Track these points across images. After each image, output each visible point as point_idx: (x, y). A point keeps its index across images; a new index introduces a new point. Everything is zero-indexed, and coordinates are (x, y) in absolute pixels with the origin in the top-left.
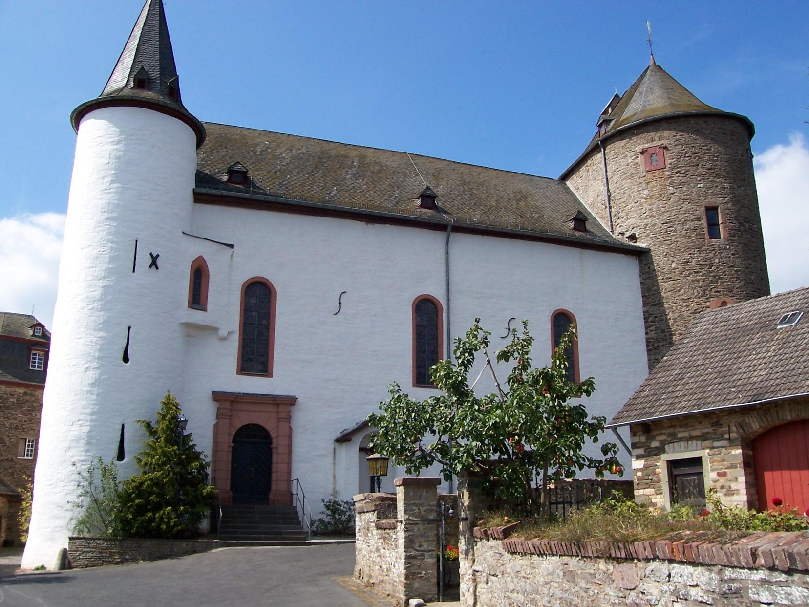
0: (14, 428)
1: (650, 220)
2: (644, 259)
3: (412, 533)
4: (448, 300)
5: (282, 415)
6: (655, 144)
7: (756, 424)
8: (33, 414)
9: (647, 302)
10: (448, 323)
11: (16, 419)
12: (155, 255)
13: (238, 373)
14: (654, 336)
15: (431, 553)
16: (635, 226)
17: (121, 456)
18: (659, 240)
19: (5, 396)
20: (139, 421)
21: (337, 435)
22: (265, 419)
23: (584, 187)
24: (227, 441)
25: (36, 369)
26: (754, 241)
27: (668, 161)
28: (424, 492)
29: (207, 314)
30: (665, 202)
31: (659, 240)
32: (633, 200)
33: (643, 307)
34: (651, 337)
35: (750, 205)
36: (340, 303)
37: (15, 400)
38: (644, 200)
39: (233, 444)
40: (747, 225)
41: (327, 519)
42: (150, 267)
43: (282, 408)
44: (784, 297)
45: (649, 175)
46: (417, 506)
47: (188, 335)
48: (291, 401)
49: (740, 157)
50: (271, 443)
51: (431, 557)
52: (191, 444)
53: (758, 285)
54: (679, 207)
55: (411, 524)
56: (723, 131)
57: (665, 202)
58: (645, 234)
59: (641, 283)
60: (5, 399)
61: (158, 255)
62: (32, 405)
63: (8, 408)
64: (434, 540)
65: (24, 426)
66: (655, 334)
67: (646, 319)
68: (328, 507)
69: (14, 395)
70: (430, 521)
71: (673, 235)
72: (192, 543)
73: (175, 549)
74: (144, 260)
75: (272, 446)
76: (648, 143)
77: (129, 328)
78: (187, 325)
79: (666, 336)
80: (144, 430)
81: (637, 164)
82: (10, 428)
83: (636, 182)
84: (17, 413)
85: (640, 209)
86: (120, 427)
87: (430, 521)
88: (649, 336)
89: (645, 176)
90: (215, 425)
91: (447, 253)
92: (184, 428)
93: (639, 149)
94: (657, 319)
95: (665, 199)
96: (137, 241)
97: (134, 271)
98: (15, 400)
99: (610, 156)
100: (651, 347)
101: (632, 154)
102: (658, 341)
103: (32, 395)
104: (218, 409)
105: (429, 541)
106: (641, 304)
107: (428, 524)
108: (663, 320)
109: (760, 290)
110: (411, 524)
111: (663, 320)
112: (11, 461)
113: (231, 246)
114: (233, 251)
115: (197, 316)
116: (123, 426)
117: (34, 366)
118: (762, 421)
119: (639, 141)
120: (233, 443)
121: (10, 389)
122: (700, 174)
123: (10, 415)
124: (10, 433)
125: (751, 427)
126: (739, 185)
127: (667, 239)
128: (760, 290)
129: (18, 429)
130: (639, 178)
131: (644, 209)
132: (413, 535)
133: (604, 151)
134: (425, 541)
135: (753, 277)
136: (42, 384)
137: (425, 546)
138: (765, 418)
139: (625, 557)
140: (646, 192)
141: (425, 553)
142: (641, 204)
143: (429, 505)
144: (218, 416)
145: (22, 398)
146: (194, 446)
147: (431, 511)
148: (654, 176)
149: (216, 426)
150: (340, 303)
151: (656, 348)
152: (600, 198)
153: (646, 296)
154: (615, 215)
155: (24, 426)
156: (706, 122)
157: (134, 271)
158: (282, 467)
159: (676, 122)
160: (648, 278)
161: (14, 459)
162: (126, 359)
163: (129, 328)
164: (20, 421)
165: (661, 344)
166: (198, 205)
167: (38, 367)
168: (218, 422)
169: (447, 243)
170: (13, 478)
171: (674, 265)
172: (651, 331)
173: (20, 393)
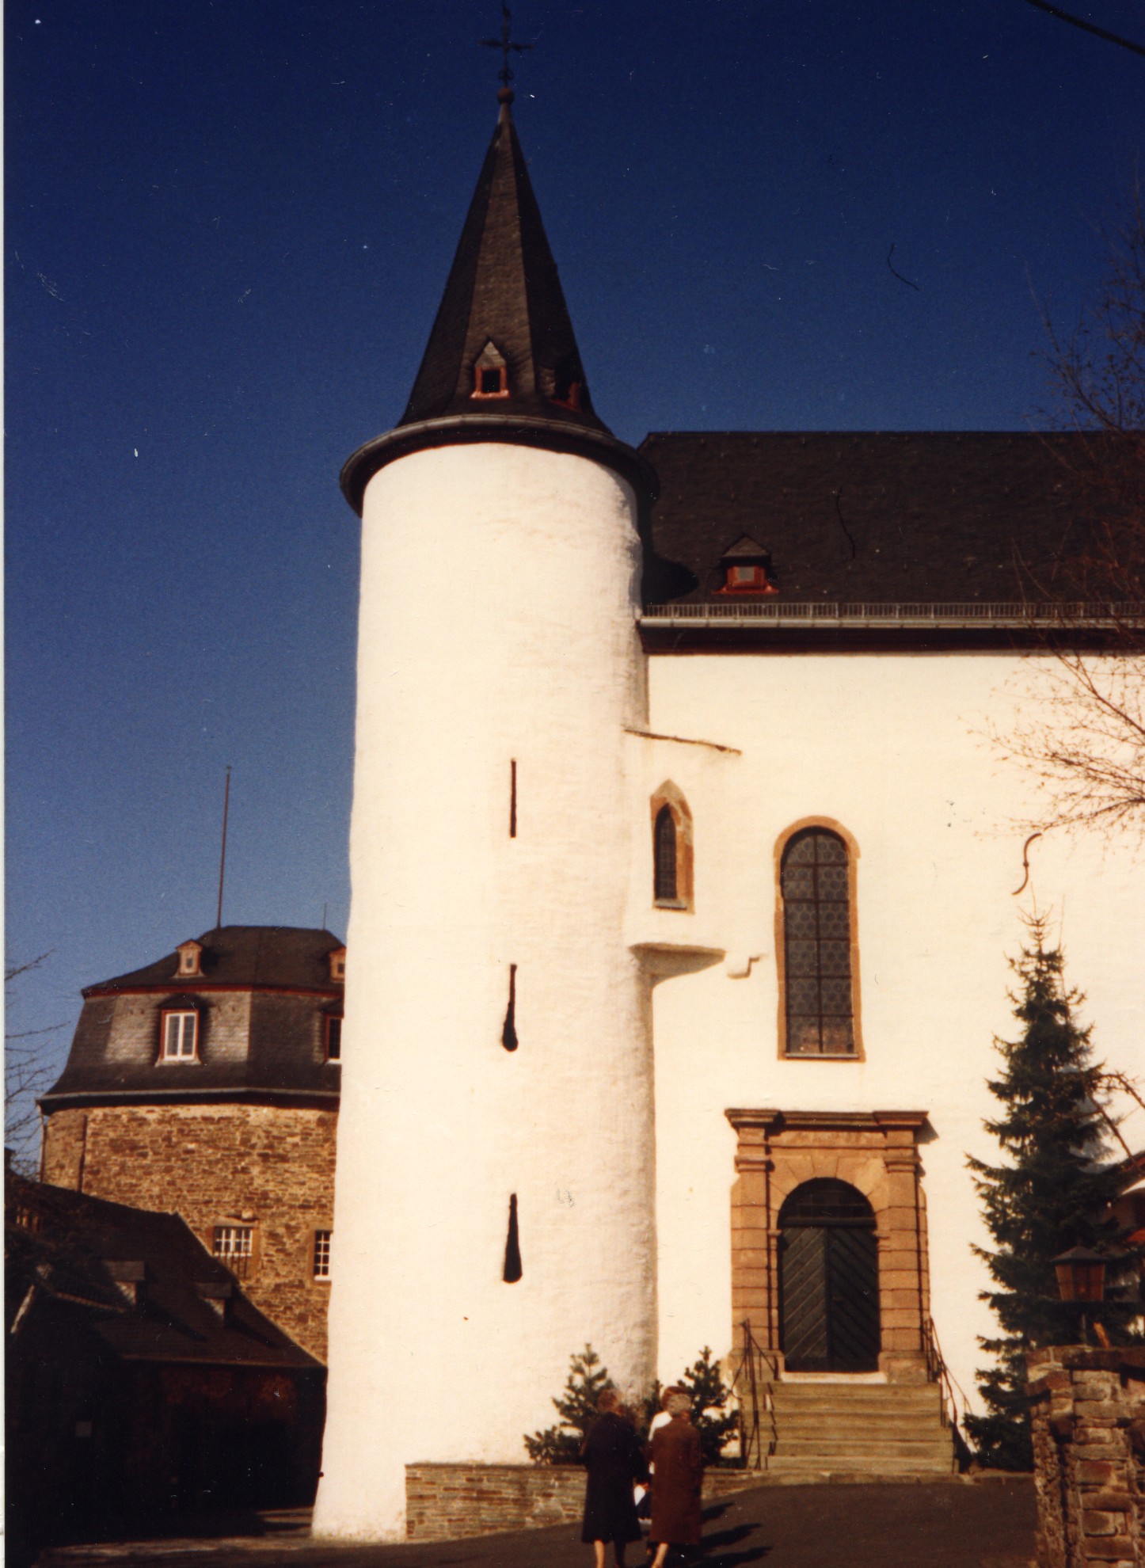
13: (860, 1058)
37: (297, 1139)
50: (874, 1226)
63: (284, 1159)
75: (877, 1233)
77: (513, 968)
86: (508, 1203)
97: (513, 833)
112: (297, 1287)
116: (514, 1200)
124: (292, 1219)
136: (329, 1094)
139: (762, 1133)
157: (513, 833)
162: (510, 1040)
163: (513, 968)
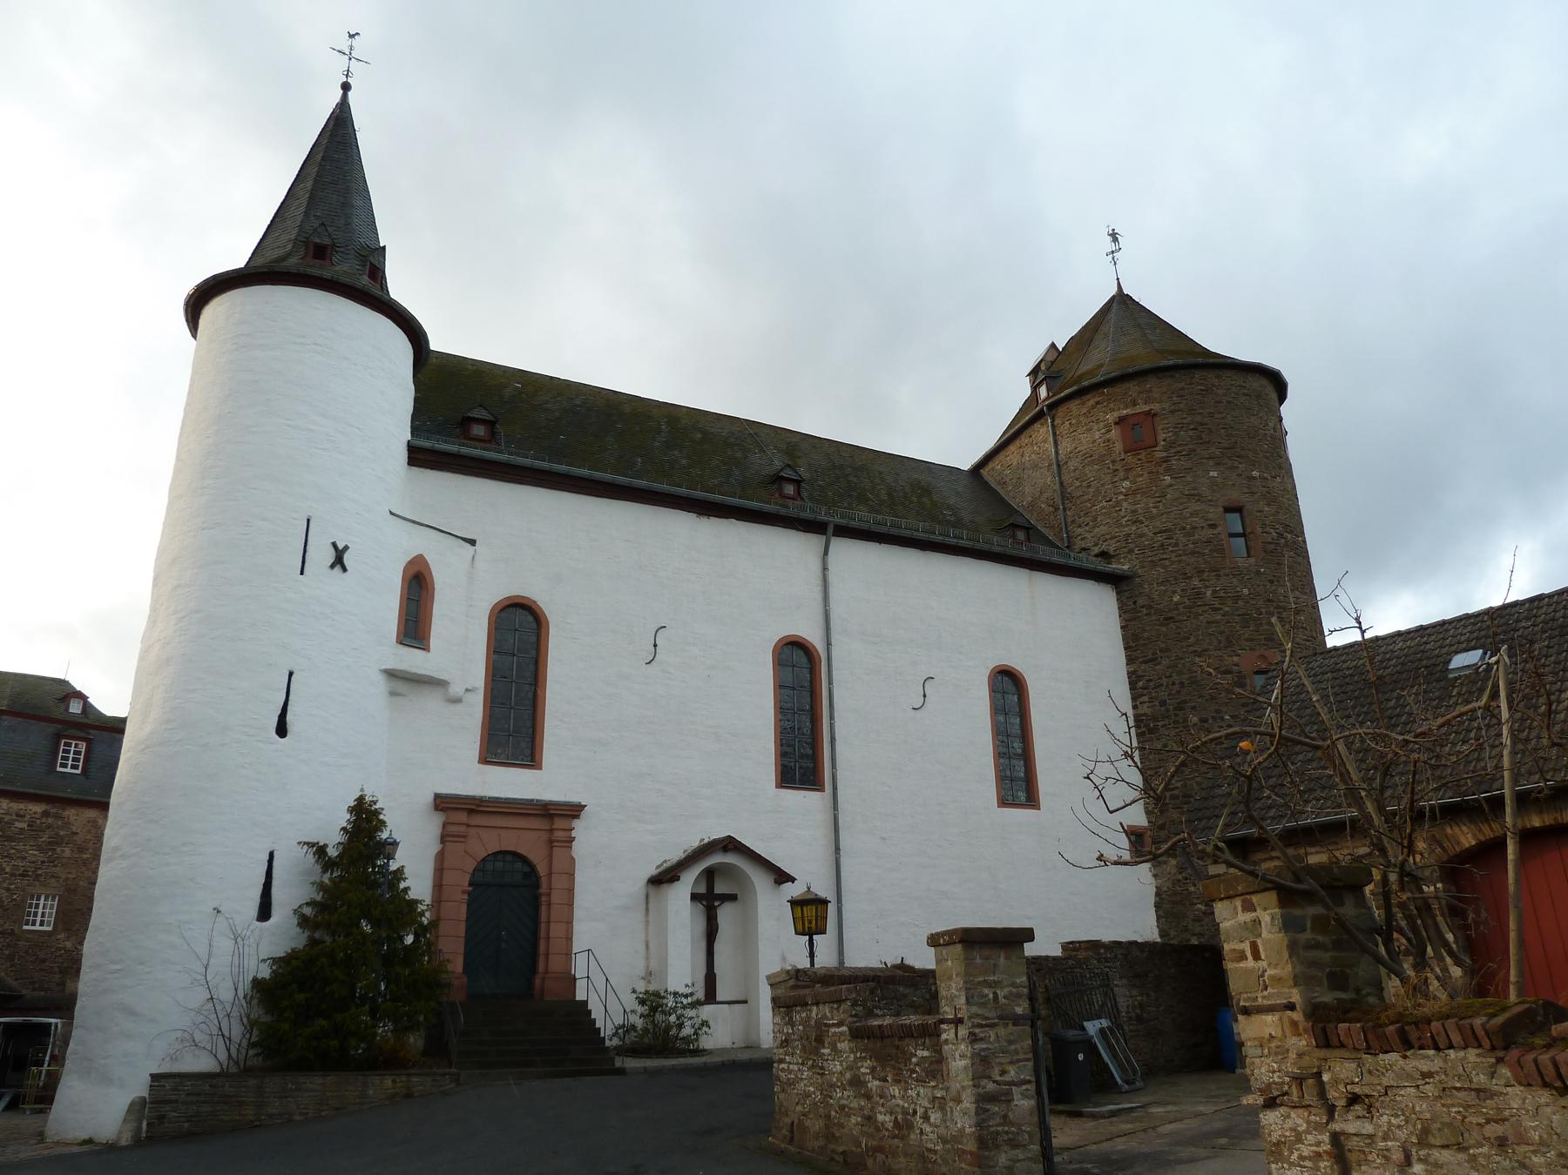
0: (20, 875)
1: (1134, 528)
2: (1125, 588)
3: (984, 1046)
4: (829, 644)
5: (559, 835)
6: (1138, 409)
7: (1469, 836)
8: (58, 850)
9: (1133, 657)
10: (830, 682)
11: (25, 858)
12: (341, 547)
14: (1148, 711)
15: (1024, 1087)
16: (1108, 537)
17: (265, 912)
18: (1150, 559)
19: (7, 818)
20: (305, 843)
21: (652, 871)
22: (528, 842)
23: (1014, 481)
24: (460, 881)
25: (68, 770)
26: (1299, 561)
27: (1161, 436)
28: (1002, 960)
29: (429, 655)
30: (1159, 499)
31: (1150, 559)
32: (1104, 497)
33: (1127, 665)
34: (1143, 712)
35: (1290, 505)
36: (655, 646)
37: (25, 825)
38: (1122, 497)
39: (471, 889)
40: (1289, 536)
41: (639, 1023)
42: (332, 566)
43: (559, 823)
44: (1434, 630)
45: (1130, 459)
46: (990, 987)
47: (393, 694)
48: (574, 811)
49: (1272, 432)
51: (1025, 1096)
52: (402, 885)
53: (1311, 631)
54: (1181, 507)
55: (981, 1026)
56: (1246, 391)
57: (1159, 499)
58: (1126, 550)
59: (1122, 627)
60: (7, 823)
61: (346, 548)
62: (57, 834)
64: (1028, 1060)
65: (40, 872)
66: (1148, 707)
67: (1133, 685)
68: (642, 1002)
69: (24, 816)
70: (1016, 1020)
71: (1172, 551)
72: (404, 1078)
73: (371, 1092)
74: (321, 555)
76: (1127, 408)
77: (291, 674)
78: (391, 674)
79: (1168, 710)
80: (311, 858)
81: (1108, 441)
82: (12, 875)
83: (1109, 468)
84: (28, 847)
85: (1116, 511)
87: (1016, 1020)
88: (1140, 711)
89: (1124, 460)
90: (437, 854)
91: (825, 569)
92: (390, 857)
93: (1111, 417)
94: (1151, 684)
95: (1157, 495)
96: (308, 520)
97: (302, 573)
98: (25, 825)
99: (1063, 429)
100: (1144, 729)
101: (1102, 425)
102: (1155, 719)
103: (57, 817)
104: (445, 825)
105: (1019, 1061)
106: (1123, 660)
107: (1014, 1025)
108: (1162, 685)
109: (1315, 639)
110: (981, 1026)
111: (1162, 685)
112: (9, 934)
113: (472, 542)
114: (475, 551)
115: (412, 660)
116: (271, 855)
117: (63, 765)
118: (1480, 830)
119: (1112, 405)
120: (470, 885)
121: (16, 806)
122: (1213, 455)
123: (12, 851)
125: (1458, 843)
126: (1273, 474)
127: (1165, 556)
128: (1315, 639)
129: (28, 876)
130: (1114, 462)
131: (1123, 510)
132: (988, 1049)
133: (1052, 422)
134: (1012, 1063)
135: (1302, 618)
137: (1012, 1073)
138: (1486, 826)
140: (1126, 484)
141: (1013, 1088)
142: (1118, 503)
143: (1013, 985)
144: (443, 839)
145: (38, 821)
146: (406, 889)
147: (1019, 996)
148: (1139, 460)
149: (440, 858)
150: (655, 646)
151: (1151, 731)
152: (1046, 495)
153: (1131, 647)
154: (1073, 522)
155: (40, 872)
156: (1218, 377)
157: (302, 573)
158: (556, 930)
159: (1172, 376)
160: (1134, 619)
161: (16, 931)
162: (282, 730)
163: (291, 674)
164: (33, 862)
165: (1160, 724)
166: (415, 470)
167: (73, 767)
168: (443, 849)
169: (826, 553)
170: (11, 966)
171: (1176, 598)
172: (1141, 703)
173: (35, 813)
